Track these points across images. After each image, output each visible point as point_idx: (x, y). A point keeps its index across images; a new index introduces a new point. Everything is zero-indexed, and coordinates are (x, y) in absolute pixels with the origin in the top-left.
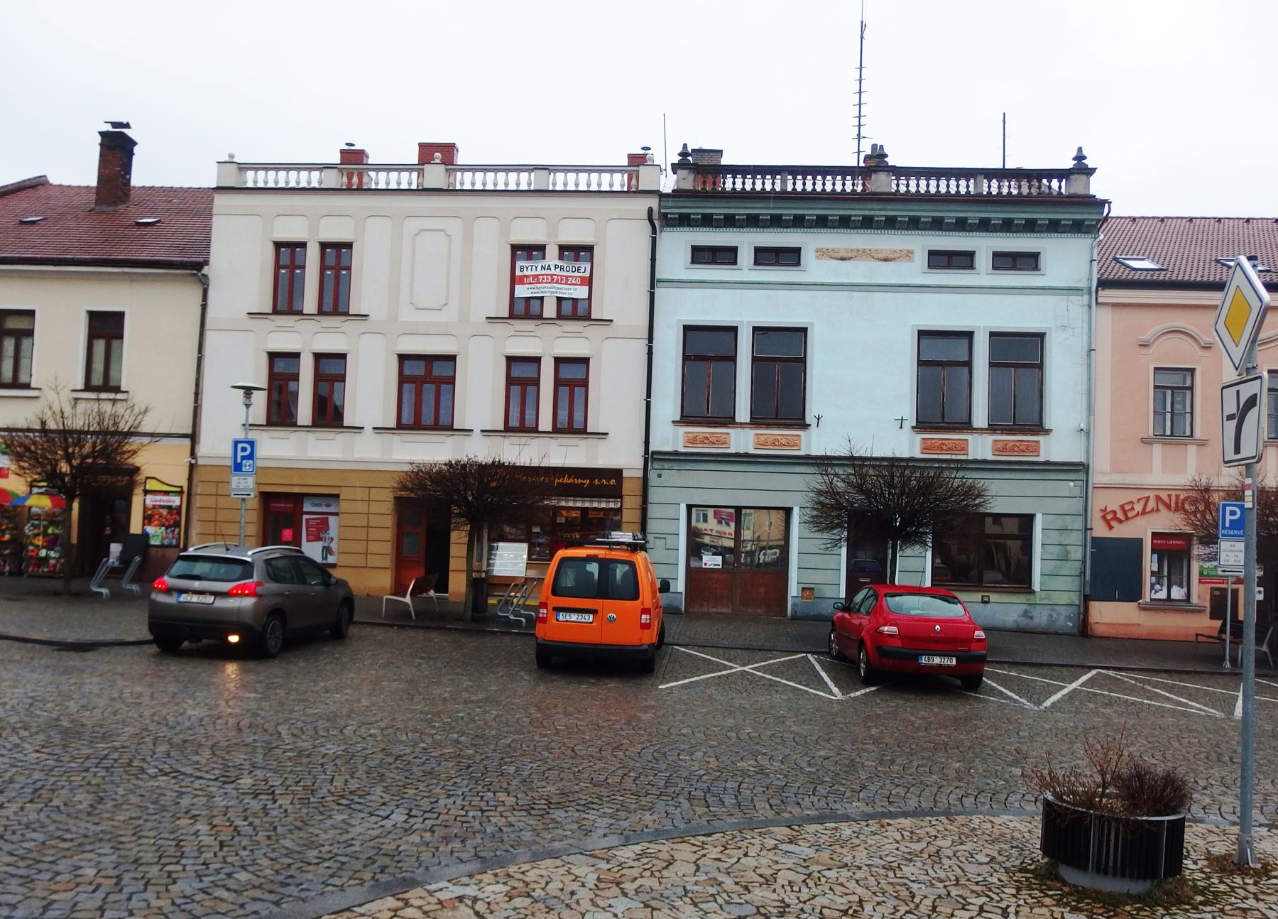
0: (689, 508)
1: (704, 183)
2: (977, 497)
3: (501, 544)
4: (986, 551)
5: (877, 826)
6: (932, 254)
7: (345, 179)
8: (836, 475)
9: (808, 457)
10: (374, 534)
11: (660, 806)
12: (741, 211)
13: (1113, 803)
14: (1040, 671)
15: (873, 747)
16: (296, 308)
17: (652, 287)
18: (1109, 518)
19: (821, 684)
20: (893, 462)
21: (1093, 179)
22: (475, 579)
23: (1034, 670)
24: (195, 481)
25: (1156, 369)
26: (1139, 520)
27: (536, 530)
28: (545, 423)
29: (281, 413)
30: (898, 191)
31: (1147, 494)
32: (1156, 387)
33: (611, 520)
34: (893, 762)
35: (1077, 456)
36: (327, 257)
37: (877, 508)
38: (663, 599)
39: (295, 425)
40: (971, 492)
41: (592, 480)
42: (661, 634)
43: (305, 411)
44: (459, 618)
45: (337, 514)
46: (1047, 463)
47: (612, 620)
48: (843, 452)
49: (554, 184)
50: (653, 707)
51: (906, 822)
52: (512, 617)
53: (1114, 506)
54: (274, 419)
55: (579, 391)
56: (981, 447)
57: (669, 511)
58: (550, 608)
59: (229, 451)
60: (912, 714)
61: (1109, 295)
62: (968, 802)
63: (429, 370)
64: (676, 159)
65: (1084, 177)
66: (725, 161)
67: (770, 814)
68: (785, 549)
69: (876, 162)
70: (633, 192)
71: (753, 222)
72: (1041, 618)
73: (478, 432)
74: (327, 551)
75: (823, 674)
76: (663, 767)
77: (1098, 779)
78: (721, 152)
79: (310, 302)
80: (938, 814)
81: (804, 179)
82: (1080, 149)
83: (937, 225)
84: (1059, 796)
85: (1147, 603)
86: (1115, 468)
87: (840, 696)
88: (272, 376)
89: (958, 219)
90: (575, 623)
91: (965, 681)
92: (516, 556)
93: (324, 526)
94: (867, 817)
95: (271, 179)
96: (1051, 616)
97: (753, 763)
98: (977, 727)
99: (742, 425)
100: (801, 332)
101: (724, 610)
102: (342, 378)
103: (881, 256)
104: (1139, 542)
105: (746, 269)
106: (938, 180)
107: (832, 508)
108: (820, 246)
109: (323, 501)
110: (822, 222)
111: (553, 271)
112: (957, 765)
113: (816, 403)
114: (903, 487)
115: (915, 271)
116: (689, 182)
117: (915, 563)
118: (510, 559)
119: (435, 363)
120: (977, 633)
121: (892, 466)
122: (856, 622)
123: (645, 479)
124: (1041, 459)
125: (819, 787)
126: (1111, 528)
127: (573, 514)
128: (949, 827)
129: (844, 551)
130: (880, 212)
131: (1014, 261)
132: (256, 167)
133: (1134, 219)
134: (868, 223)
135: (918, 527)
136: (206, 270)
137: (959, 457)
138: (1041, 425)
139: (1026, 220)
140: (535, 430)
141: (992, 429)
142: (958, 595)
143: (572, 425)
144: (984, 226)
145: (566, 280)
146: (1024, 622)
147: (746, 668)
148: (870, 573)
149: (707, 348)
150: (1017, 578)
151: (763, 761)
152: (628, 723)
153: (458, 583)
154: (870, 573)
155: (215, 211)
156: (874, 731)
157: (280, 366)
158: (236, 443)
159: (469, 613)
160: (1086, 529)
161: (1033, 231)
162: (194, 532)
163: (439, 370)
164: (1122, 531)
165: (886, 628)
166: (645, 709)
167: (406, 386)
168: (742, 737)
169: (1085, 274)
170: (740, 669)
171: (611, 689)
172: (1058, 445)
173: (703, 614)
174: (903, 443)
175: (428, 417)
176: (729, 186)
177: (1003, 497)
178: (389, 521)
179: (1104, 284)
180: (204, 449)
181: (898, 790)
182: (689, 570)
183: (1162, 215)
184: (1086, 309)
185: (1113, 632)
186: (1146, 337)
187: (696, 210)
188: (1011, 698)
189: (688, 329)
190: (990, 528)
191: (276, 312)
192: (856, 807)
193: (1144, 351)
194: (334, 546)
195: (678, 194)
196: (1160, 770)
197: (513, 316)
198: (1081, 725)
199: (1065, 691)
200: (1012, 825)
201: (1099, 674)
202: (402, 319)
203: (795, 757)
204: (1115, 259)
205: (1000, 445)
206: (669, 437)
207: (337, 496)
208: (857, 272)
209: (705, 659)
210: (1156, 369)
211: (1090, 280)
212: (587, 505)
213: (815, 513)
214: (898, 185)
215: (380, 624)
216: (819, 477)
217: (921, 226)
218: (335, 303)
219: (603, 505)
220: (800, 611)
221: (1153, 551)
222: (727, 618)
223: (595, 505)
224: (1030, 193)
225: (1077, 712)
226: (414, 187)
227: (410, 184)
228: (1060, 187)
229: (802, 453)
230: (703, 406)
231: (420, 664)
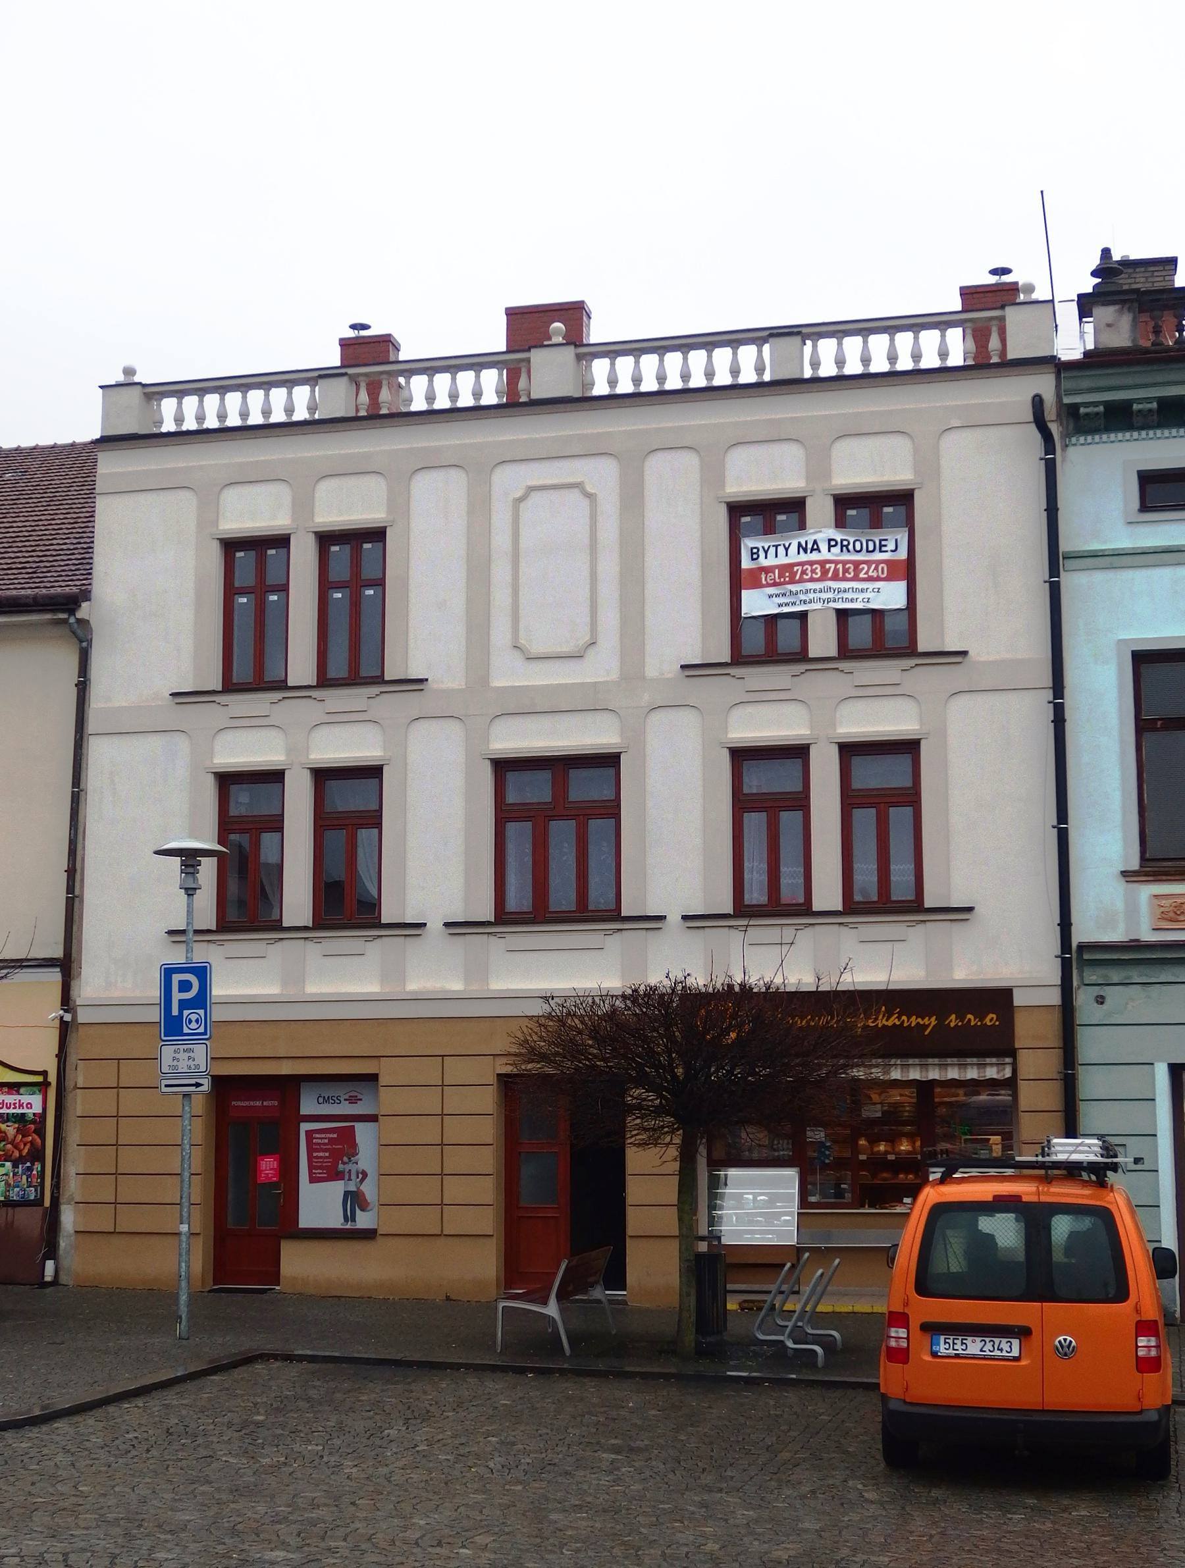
3: (733, 1172)
7: (364, 397)
10: (456, 1160)
16: (271, 675)
17: (1054, 569)
22: (699, 1256)
24: (72, 1059)
27: (817, 1135)
28: (827, 892)
29: (246, 905)
36: (332, 564)
39: (277, 926)
41: (941, 1018)
43: (297, 897)
44: (665, 1348)
45: (373, 1118)
47: (1065, 1352)
49: (815, 364)
52: (790, 1344)
54: (232, 915)
55: (899, 816)
58: (915, 1323)
59: (154, 992)
63: (560, 788)
64: (1088, 284)
70: (984, 365)
73: (676, 923)
74: (354, 1200)
79: (301, 663)
88: (226, 825)
89: (1110, 407)
90: (975, 1362)
92: (773, 1200)
93: (345, 1143)
95: (211, 411)
102: (374, 820)
109: (341, 1091)
111: (824, 554)
118: (759, 1206)
119: (573, 773)
123: (1067, 1008)
127: (896, 1096)
132: (179, 389)
136: (84, 611)
140: (804, 910)
143: (890, 894)
145: (854, 571)
153: (653, 1271)
155: (99, 488)
157: (243, 801)
158: (168, 972)
159: (690, 1338)
162: (71, 1170)
163: (584, 788)
167: (512, 828)
175: (562, 895)
178: (488, 1130)
180: (92, 985)
187: (1144, 391)
191: (230, 686)
194: (369, 1189)
195: (1094, 360)
197: (739, 658)
202: (498, 682)
206: (1113, 906)
207: (374, 1078)
212: (934, 1074)
215: (494, 1368)
218: (356, 659)
223: (953, 1074)
231: (613, 1467)
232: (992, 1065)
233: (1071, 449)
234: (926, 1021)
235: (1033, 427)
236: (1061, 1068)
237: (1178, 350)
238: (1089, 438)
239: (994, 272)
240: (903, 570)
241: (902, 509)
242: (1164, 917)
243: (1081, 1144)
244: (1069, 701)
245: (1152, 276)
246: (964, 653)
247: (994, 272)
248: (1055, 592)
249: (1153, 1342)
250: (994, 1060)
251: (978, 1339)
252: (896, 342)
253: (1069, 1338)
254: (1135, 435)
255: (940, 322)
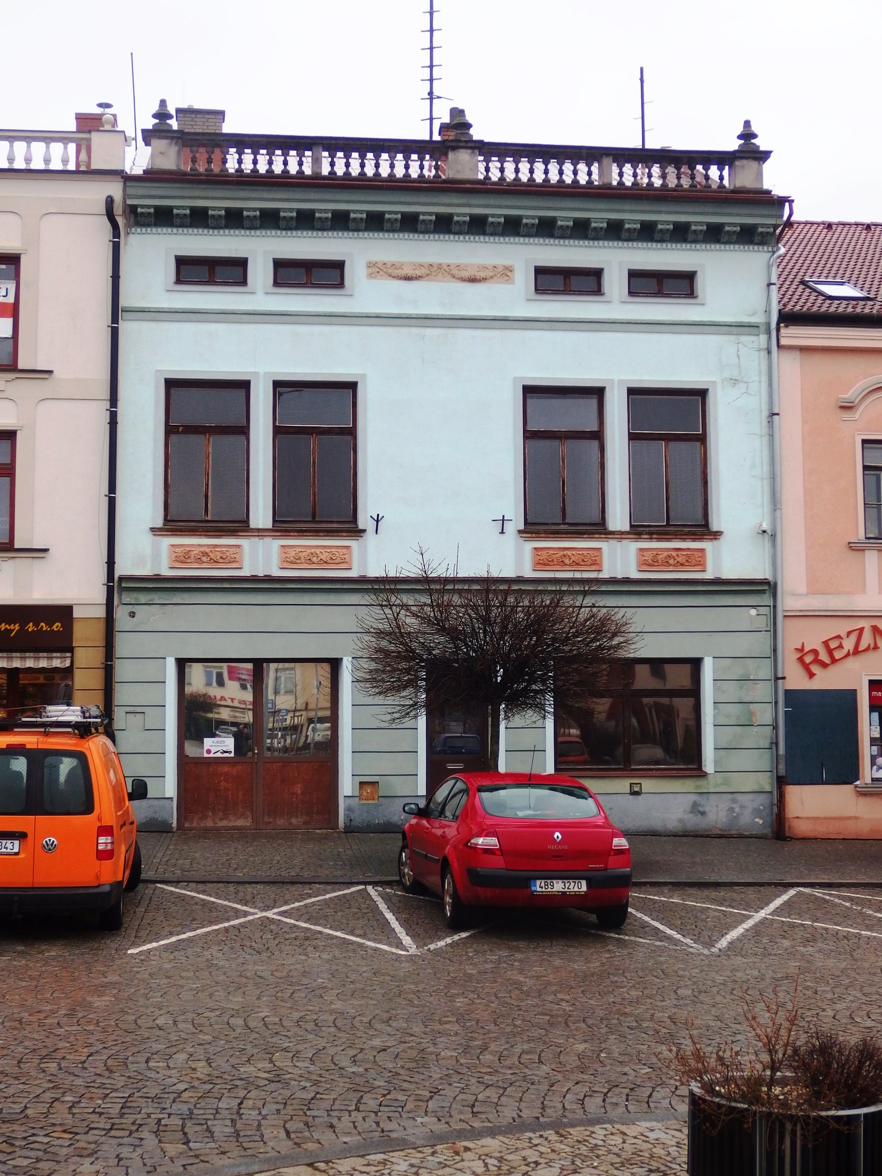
0: (182, 664)
1: (194, 160)
2: (615, 635)
4: (636, 718)
5: (449, 1153)
6: (540, 271)
8: (403, 606)
9: (363, 580)
11: (109, 1148)
12: (252, 203)
13: (786, 1093)
14: (713, 894)
15: (456, 1027)
17: (115, 318)
18: (809, 661)
19: (385, 932)
20: (488, 585)
21: (767, 166)
23: (706, 892)
25: (864, 442)
26: (852, 664)
30: (487, 178)
31: (861, 624)
32: (866, 468)
33: (55, 686)
34: (484, 1048)
35: (757, 570)
37: (473, 657)
38: (139, 810)
40: (602, 628)
42: (135, 866)
46: (717, 581)
47: (49, 849)
48: (412, 570)
50: (113, 984)
51: (492, 1144)
53: (814, 642)
56: (620, 559)
57: (146, 670)
60: (521, 971)
61: (795, 335)
62: (594, 1105)
64: (149, 123)
65: (754, 164)
66: (228, 127)
67: (285, 1146)
68: (334, 719)
69: (456, 134)
70: (86, 173)
71: (270, 220)
72: (717, 815)
75: (389, 916)
76: (120, 1082)
77: (765, 1057)
78: (222, 113)
80: (544, 1127)
81: (347, 157)
82: (747, 124)
83: (546, 229)
84: (709, 1088)
85: (866, 786)
86: (814, 588)
87: (413, 950)
89: (439, 216)
91: (601, 915)
94: (435, 1139)
96: (731, 810)
97: (268, 1066)
98: (616, 985)
99: (261, 532)
100: (699, 395)
101: (240, 823)
103: (466, 274)
104: (852, 694)
105: (260, 292)
106: (546, 163)
107: (400, 657)
108: (375, 258)
110: (375, 223)
112: (581, 1047)
113: (373, 497)
114: (504, 627)
115: (516, 296)
116: (170, 158)
117: (528, 738)
120: (616, 841)
121: (488, 591)
122: (439, 832)
124: (709, 575)
125: (367, 1098)
126: (811, 675)
128: (558, 1146)
129: (422, 722)
130: (462, 209)
131: (660, 284)
133: (829, 226)
134: (444, 225)
135: (530, 683)
137: (586, 575)
138: (706, 525)
139: (742, 226)
141: (636, 531)
142: (588, 783)
144: (615, 232)
146: (693, 822)
147: (269, 914)
148: (463, 755)
149: (202, 413)
150: (682, 754)
151: (282, 1060)
152: (71, 1014)
154: (463, 755)
156: (460, 1002)
160: (777, 679)
161: (685, 240)
164: (827, 680)
165: (480, 840)
166: (100, 990)
168: (252, 1024)
169: (762, 307)
170: (260, 915)
171: (50, 960)
172: (732, 556)
173: (207, 830)
174: (507, 557)
176: (232, 165)
177: (653, 633)
179: (788, 318)
181: (488, 1092)
182: (183, 760)
183: (868, 221)
184: (764, 354)
185: (821, 830)
186: (850, 394)
188: (669, 938)
189: (171, 385)
190: (643, 679)
192: (424, 1124)
193: (846, 415)
195: (151, 176)
196: (851, 1038)
198: (769, 974)
199: (749, 923)
200: (652, 1136)
201: (799, 894)
203: (332, 1051)
204: (802, 282)
205: (648, 556)
206: (145, 551)
208: (427, 297)
209: (205, 903)
210: (864, 442)
211: (768, 312)
212: (16, 664)
213: (373, 666)
214: (487, 169)
216: (378, 610)
217: (522, 230)
219: (43, 664)
220: (359, 818)
221: (872, 709)
222: (241, 835)
223: (30, 663)
224: (679, 185)
225: (766, 954)
226: (72, 166)
227: (65, 161)
228: (721, 178)
229: (353, 574)
230: (199, 506)
232: (57, 657)
233: (131, 236)
234: (12, 627)
235: (106, 218)
236: (104, 661)
237: (206, 176)
238: (144, 230)
239: (100, 105)
240: (10, 310)
241: (13, 267)
242: (177, 559)
243: (67, 710)
244: (121, 410)
245: (204, 122)
246: (51, 372)
247: (100, 105)
248: (115, 334)
249: (109, 839)
250: (58, 655)
251: (560, 881)
252: (32, 149)
253: (52, 839)
254: (175, 230)
255: (62, 138)
